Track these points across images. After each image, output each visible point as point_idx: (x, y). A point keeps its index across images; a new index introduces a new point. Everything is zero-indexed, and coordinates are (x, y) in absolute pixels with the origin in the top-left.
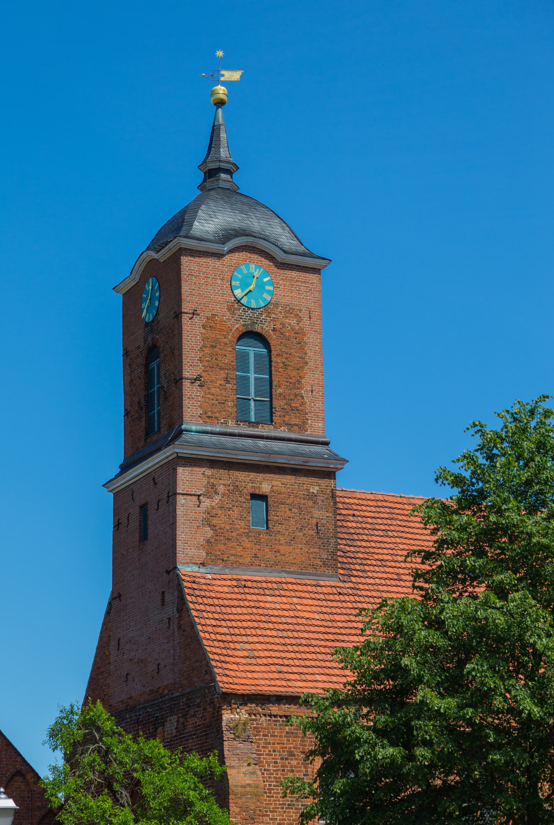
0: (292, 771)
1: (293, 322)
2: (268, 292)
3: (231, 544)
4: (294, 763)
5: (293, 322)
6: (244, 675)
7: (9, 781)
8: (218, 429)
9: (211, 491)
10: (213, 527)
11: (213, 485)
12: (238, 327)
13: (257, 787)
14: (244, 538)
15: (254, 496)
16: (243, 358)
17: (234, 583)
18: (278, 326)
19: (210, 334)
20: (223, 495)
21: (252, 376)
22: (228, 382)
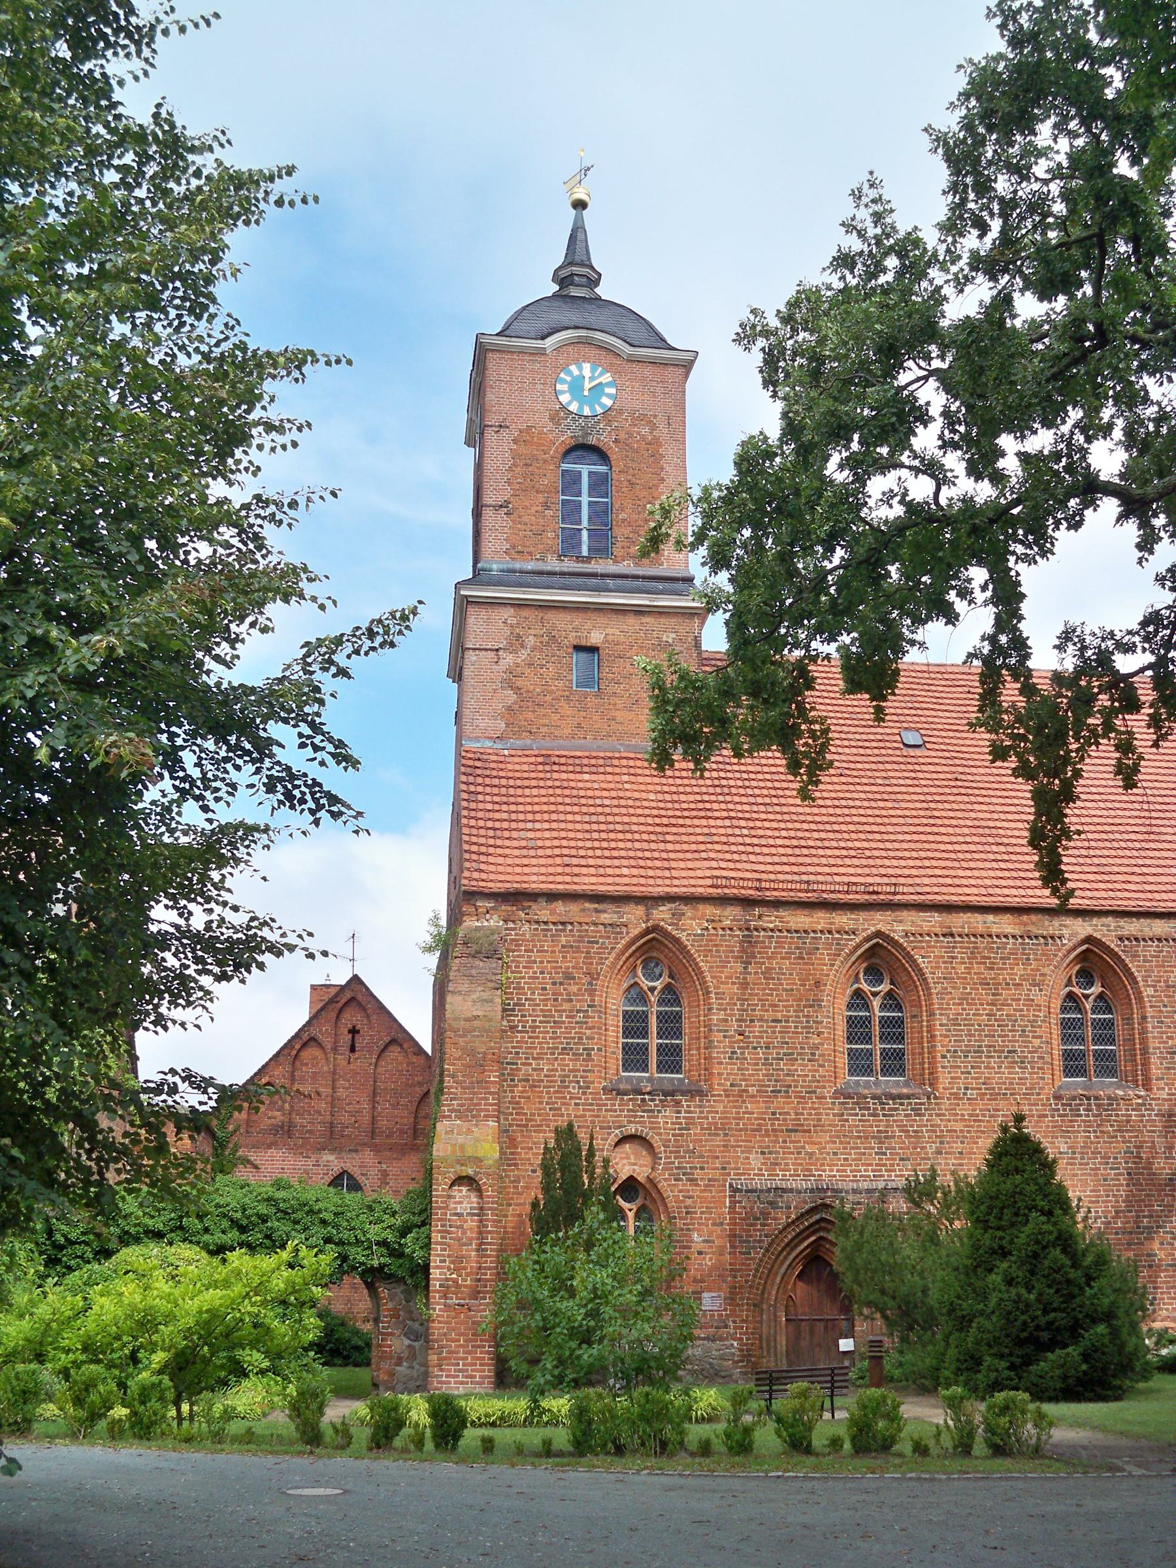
0: (571, 1001)
1: (645, 430)
2: (609, 396)
3: (541, 711)
4: (574, 988)
5: (645, 430)
6: (509, 870)
7: (383, 1051)
8: (530, 566)
9: (516, 643)
10: (517, 690)
11: (519, 636)
12: (566, 438)
13: (490, 1020)
14: (563, 703)
15: (578, 648)
16: (571, 482)
17: (540, 759)
18: (623, 436)
19: (523, 450)
20: (533, 649)
21: (585, 499)
22: (548, 508)
